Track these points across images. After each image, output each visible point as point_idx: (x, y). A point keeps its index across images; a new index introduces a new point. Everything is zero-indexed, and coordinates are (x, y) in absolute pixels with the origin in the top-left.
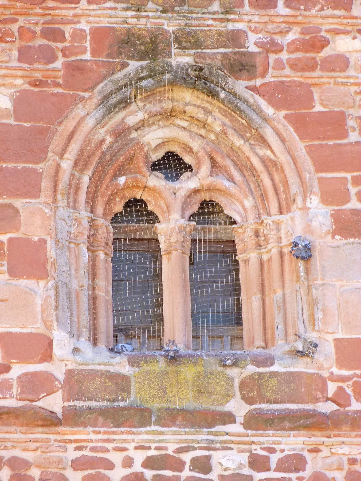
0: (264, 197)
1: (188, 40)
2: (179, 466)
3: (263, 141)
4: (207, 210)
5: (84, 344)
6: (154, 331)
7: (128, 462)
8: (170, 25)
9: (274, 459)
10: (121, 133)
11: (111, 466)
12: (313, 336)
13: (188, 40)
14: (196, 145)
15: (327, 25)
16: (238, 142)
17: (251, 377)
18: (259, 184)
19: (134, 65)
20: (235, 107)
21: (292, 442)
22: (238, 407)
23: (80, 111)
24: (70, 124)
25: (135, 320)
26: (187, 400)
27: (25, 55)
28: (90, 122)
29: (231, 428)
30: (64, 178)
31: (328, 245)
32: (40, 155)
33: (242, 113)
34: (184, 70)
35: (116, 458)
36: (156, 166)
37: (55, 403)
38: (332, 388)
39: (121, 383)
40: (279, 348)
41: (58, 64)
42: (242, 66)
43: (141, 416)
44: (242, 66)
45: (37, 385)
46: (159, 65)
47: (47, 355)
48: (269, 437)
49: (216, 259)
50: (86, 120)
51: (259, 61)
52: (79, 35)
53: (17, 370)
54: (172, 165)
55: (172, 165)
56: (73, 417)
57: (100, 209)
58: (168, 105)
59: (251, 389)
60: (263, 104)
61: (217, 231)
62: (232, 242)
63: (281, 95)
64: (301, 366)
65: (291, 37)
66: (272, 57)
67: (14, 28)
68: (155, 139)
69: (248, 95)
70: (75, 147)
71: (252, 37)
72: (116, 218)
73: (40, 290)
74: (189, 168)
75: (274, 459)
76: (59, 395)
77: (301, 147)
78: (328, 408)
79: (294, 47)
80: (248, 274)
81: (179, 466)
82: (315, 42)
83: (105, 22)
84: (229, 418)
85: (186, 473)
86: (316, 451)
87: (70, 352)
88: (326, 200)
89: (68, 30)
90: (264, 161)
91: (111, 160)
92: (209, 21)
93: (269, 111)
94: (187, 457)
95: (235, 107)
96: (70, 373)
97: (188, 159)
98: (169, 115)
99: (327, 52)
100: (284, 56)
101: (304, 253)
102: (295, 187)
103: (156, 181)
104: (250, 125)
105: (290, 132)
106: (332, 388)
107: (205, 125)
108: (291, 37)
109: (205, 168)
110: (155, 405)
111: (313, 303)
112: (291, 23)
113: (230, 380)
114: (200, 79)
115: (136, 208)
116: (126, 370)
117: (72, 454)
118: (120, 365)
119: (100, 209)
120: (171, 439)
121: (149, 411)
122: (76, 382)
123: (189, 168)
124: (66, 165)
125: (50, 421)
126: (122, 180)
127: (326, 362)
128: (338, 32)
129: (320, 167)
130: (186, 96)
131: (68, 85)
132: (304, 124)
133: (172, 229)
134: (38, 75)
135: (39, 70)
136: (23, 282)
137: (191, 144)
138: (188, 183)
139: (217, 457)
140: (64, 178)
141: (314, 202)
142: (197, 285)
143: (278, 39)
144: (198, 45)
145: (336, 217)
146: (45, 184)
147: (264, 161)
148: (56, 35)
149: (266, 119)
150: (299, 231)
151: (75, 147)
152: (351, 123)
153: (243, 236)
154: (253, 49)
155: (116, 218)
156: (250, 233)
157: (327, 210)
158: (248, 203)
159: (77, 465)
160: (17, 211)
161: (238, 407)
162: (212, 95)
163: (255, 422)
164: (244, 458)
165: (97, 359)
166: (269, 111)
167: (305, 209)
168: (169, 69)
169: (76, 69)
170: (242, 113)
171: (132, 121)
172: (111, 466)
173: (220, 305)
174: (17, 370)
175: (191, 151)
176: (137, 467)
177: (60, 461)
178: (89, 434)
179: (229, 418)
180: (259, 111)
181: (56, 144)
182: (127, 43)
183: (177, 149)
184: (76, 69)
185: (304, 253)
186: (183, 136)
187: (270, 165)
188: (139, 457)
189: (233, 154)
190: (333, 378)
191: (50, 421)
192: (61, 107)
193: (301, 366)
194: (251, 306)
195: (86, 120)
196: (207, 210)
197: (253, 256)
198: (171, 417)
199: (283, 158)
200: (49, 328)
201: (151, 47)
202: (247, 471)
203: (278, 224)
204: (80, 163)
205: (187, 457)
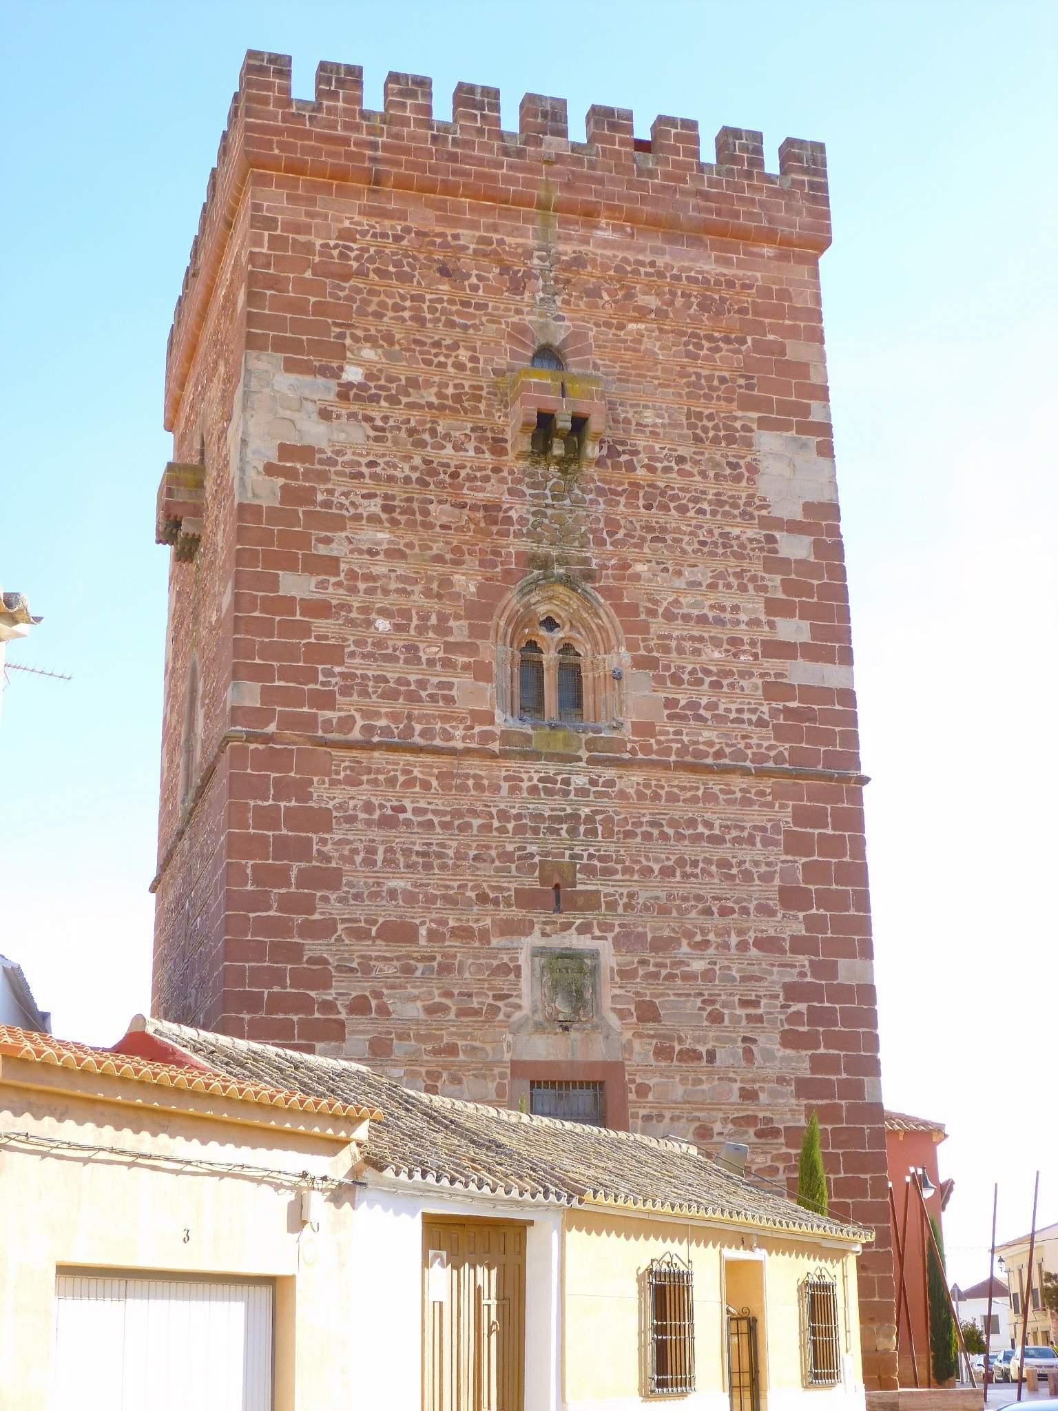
0: (596, 644)
1: (563, 561)
2: (555, 782)
3: (598, 616)
4: (566, 648)
5: (509, 717)
6: (539, 707)
7: (530, 779)
8: (554, 553)
9: (601, 780)
10: (527, 606)
11: (522, 780)
12: (621, 719)
13: (563, 561)
14: (563, 614)
15: (631, 556)
16: (585, 615)
17: (591, 739)
18: (595, 638)
19: (536, 572)
20: (585, 597)
21: (610, 773)
22: (584, 754)
23: (509, 595)
24: (504, 602)
25: (532, 705)
26: (560, 749)
27: (482, 563)
28: (514, 601)
29: (580, 764)
30: (501, 630)
31: (629, 672)
32: (489, 617)
33: (588, 601)
34: (560, 576)
35: (525, 776)
36: (542, 623)
37: (495, 746)
38: (629, 746)
39: (528, 739)
40: (603, 723)
41: (498, 569)
42: (589, 576)
43: (536, 756)
44: (589, 576)
45: (487, 737)
46: (548, 573)
47: (492, 722)
48: (599, 770)
49: (571, 674)
50: (512, 601)
51: (598, 573)
52: (509, 555)
53: (477, 729)
54: (550, 624)
55: (550, 624)
56: (504, 755)
57: (515, 645)
58: (551, 594)
59: (591, 745)
60: (599, 596)
61: (571, 659)
62: (579, 666)
63: (608, 592)
64: (615, 735)
65: (613, 562)
66: (604, 572)
67: (477, 548)
68: (543, 610)
69: (589, 589)
70: (506, 614)
71: (594, 561)
72: (522, 650)
73: (489, 688)
74: (558, 626)
75: (601, 780)
76: (498, 742)
77: (617, 620)
78: (627, 756)
79: (614, 567)
80: (587, 684)
81: (555, 782)
82: (625, 566)
83: (522, 549)
84: (579, 759)
85: (559, 785)
86: (621, 778)
87: (503, 721)
88: (628, 649)
89: (503, 552)
90: (597, 625)
91: (521, 621)
92: (573, 552)
93: (602, 601)
94: (559, 778)
95: (585, 597)
96: (502, 732)
97: (557, 621)
98: (551, 598)
99: (630, 571)
100: (610, 572)
101: (618, 677)
102: (614, 642)
103: (543, 632)
104: (591, 608)
105: (612, 612)
106: (629, 746)
107: (568, 604)
108: (613, 562)
109: (567, 627)
110: (544, 751)
111: (621, 703)
112: (613, 555)
113: (580, 740)
114: (568, 581)
115: (532, 645)
116: (530, 732)
117: (504, 773)
118: (527, 729)
119: (515, 645)
120: (551, 768)
121: (541, 753)
122: (506, 736)
123: (558, 626)
124: (502, 623)
125: (493, 756)
126: (527, 631)
127: (627, 733)
128: (636, 561)
129: (627, 631)
130: (561, 589)
131: (504, 580)
132: (618, 608)
133: (550, 657)
134: (489, 575)
135: (490, 572)
136: (481, 684)
137: (561, 614)
138: (559, 634)
139: (573, 778)
140: (501, 630)
141: (623, 649)
142: (561, 688)
143: (607, 563)
144: (567, 563)
145: (633, 658)
146: (492, 633)
147: (597, 625)
148: (497, 553)
149: (600, 605)
150: (615, 666)
151: (506, 614)
152: (641, 609)
153: (585, 663)
154: (594, 567)
155: (522, 650)
156: (589, 662)
157: (629, 654)
158: (588, 647)
159: (506, 779)
160: (478, 647)
161: (584, 754)
162: (574, 590)
163: (592, 761)
164: (586, 780)
165: (514, 725)
166: (602, 601)
167: (619, 653)
168: (553, 575)
169: (507, 573)
170: (588, 601)
171: (533, 601)
172: (522, 780)
173: (573, 697)
174: (477, 729)
175: (560, 617)
176: (535, 782)
177: (498, 777)
178: (513, 764)
179: (579, 759)
180: (597, 601)
181: (497, 612)
182: (533, 560)
183: (553, 616)
184: (507, 573)
185: (618, 677)
186: (557, 609)
187: (600, 628)
188: (536, 777)
189: (582, 621)
190: (630, 741)
191: (493, 756)
192: (501, 593)
193: (615, 735)
194: (588, 700)
195: (512, 601)
196: (566, 648)
197: (590, 675)
198: (551, 757)
199: (609, 626)
200: (493, 708)
201: (544, 563)
202: (587, 786)
203: (604, 660)
204: (508, 624)
205: (559, 778)
